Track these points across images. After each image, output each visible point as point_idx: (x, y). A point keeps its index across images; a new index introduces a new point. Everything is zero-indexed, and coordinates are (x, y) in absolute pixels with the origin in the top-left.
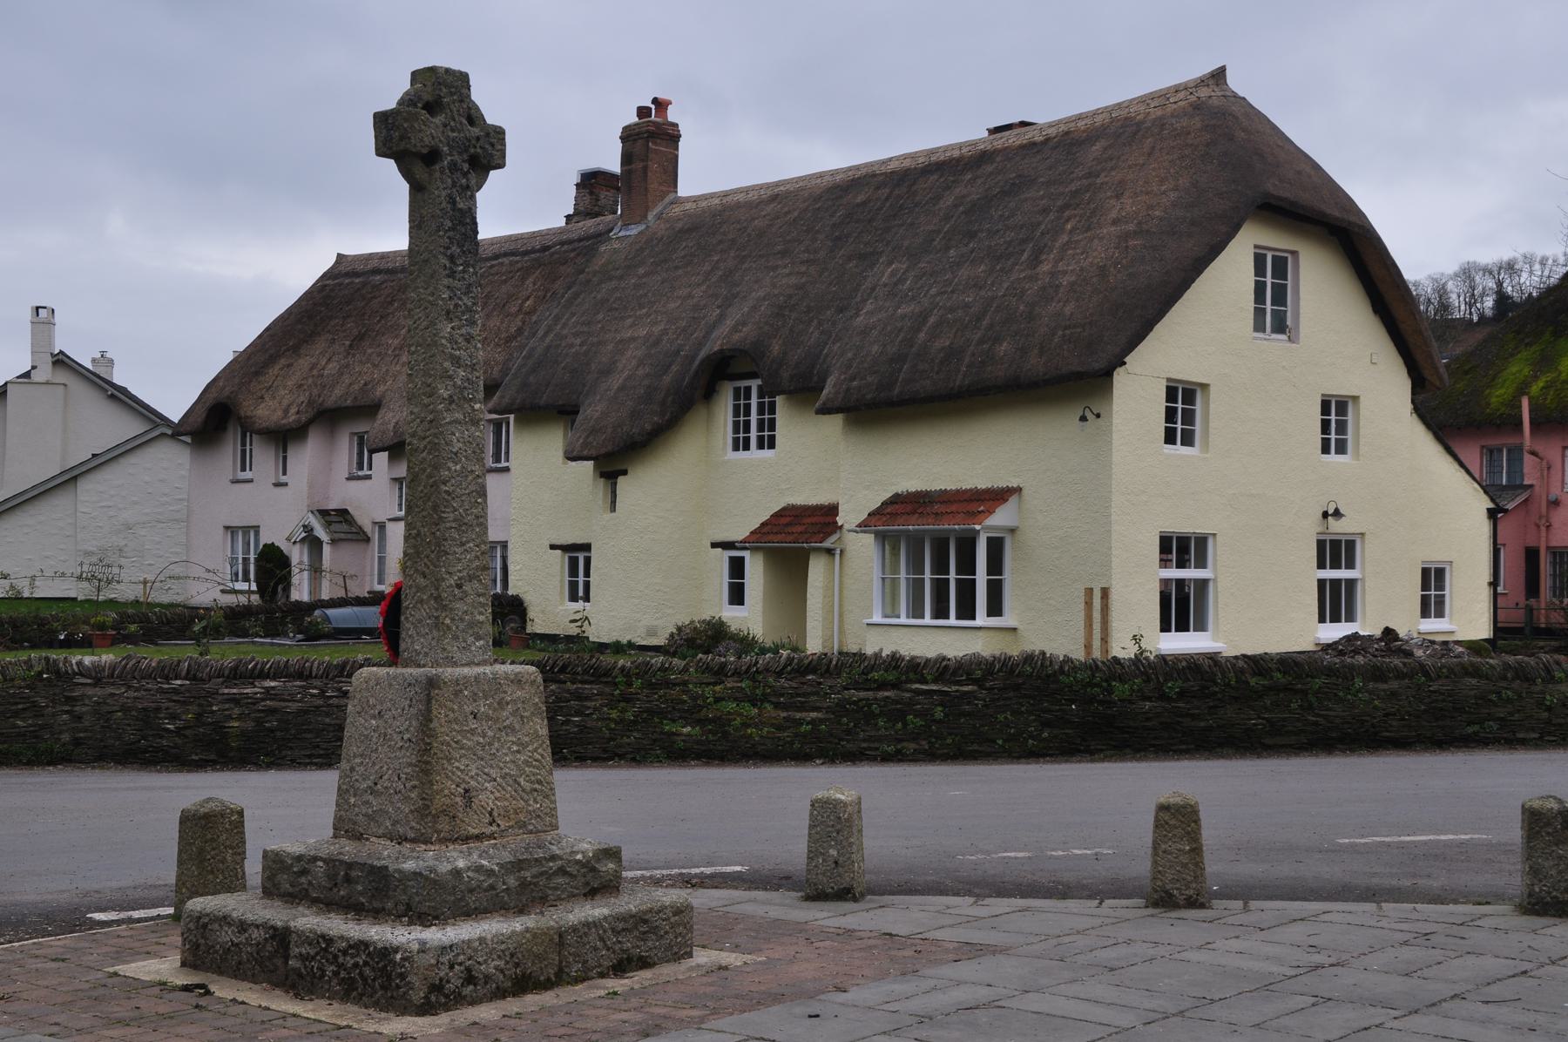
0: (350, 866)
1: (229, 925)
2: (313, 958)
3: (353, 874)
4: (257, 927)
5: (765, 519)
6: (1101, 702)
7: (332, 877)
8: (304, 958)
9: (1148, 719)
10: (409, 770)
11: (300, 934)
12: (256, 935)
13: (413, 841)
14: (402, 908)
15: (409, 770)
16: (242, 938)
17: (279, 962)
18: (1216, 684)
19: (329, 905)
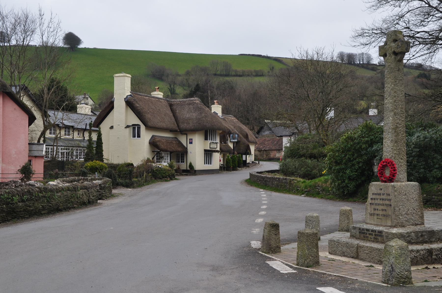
0: (423, 232)
1: (413, 252)
2: (439, 254)
3: (424, 234)
4: (423, 250)
5: (102, 136)
6: (11, 204)
7: (417, 236)
8: (436, 255)
9: (21, 208)
10: (417, 207)
11: (435, 249)
12: (422, 252)
13: (419, 225)
14: (437, 239)
15: (417, 207)
16: (418, 254)
17: (430, 258)
18: (33, 196)
19: (417, 243)
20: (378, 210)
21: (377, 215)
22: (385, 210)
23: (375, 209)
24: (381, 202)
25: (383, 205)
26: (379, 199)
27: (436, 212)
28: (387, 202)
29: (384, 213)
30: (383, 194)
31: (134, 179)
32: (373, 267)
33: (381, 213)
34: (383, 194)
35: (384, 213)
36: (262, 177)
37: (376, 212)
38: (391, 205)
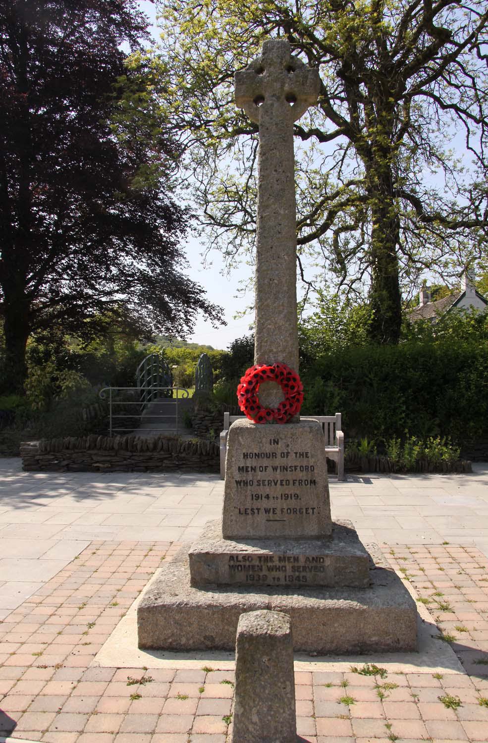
20: (268, 497)
21: (267, 511)
22: (297, 496)
23: (258, 497)
24: (278, 475)
25: (284, 483)
26: (270, 469)
27: (104, 476)
28: (302, 475)
29: (292, 503)
30: (285, 455)
31: (337, 450)
32: (382, 672)
33: (279, 504)
34: (285, 455)
35: (292, 503)
36: (258, 345)
37: (264, 504)
38: (313, 482)
